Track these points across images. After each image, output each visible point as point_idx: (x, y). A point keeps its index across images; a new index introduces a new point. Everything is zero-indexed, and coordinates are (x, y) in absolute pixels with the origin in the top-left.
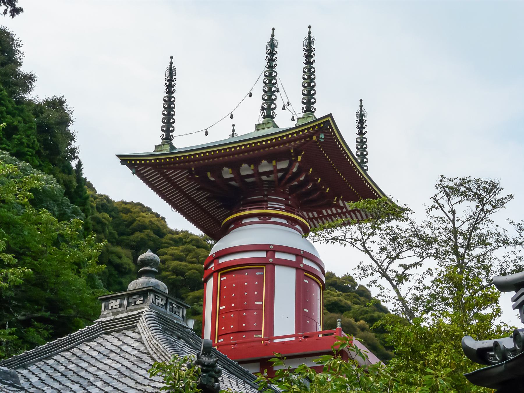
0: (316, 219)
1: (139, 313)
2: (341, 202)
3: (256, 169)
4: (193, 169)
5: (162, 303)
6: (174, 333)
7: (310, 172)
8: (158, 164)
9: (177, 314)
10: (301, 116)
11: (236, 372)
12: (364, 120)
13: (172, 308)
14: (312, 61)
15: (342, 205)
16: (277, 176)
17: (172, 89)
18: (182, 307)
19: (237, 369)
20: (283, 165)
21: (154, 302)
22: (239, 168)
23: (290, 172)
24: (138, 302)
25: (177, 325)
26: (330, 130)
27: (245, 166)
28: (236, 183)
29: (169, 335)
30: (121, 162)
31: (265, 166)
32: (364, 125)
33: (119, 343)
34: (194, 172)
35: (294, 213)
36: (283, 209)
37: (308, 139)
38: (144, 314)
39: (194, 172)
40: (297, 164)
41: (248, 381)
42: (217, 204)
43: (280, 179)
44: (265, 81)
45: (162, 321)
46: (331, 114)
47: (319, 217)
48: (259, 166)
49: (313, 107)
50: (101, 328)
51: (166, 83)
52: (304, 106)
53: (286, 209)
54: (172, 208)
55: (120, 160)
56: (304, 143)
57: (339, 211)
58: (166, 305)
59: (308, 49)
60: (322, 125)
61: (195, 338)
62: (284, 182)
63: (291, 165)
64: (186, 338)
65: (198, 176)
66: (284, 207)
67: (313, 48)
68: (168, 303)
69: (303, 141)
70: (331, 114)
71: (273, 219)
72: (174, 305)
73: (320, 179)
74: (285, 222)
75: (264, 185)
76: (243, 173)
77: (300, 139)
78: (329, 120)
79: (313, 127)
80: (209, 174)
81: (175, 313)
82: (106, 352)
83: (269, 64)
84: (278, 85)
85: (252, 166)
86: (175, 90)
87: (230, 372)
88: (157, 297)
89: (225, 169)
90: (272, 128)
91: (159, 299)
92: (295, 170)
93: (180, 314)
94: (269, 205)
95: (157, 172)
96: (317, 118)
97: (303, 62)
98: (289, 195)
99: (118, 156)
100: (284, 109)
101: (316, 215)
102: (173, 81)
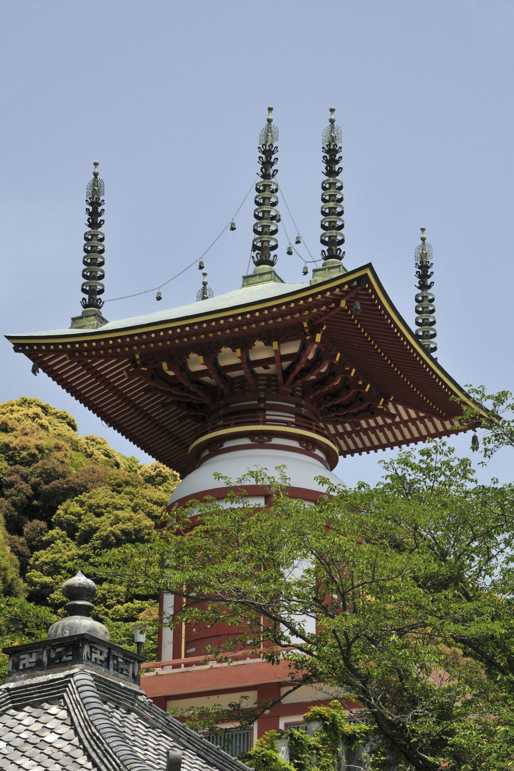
1: (67, 677)
3: (245, 356)
4: (137, 357)
5: (102, 658)
6: (120, 704)
7: (337, 359)
8: (78, 350)
9: (125, 672)
11: (218, 762)
13: (118, 664)
14: (336, 170)
15: (393, 411)
16: (281, 367)
17: (99, 219)
18: (132, 661)
19: (219, 756)
21: (90, 657)
23: (303, 360)
25: (125, 691)
26: (370, 291)
30: (14, 348)
31: (259, 350)
32: (430, 271)
34: (138, 362)
35: (310, 430)
36: (292, 423)
37: (333, 305)
38: (76, 678)
39: (138, 362)
40: (315, 346)
42: (180, 413)
43: (286, 373)
44: (257, 200)
45: (102, 687)
46: (371, 263)
48: (250, 351)
49: (339, 249)
50: (7, 700)
53: (297, 423)
55: (14, 344)
56: (325, 312)
57: (389, 421)
58: (107, 660)
60: (355, 283)
61: (153, 710)
62: (292, 376)
64: (140, 711)
65: (146, 369)
66: (294, 420)
68: (111, 657)
69: (324, 308)
70: (371, 263)
71: (276, 441)
73: (354, 370)
74: (295, 444)
75: (260, 382)
76: (224, 362)
77: (318, 305)
78: (366, 275)
80: (165, 366)
82: (18, 742)
83: (263, 170)
84: (280, 209)
85: (238, 351)
86: (103, 221)
88: (93, 650)
89: (193, 356)
90: (271, 284)
91: (96, 651)
92: (311, 356)
93: (129, 673)
94: (267, 417)
96: (349, 270)
97: (322, 172)
98: (303, 398)
99: (9, 338)
100: (290, 253)
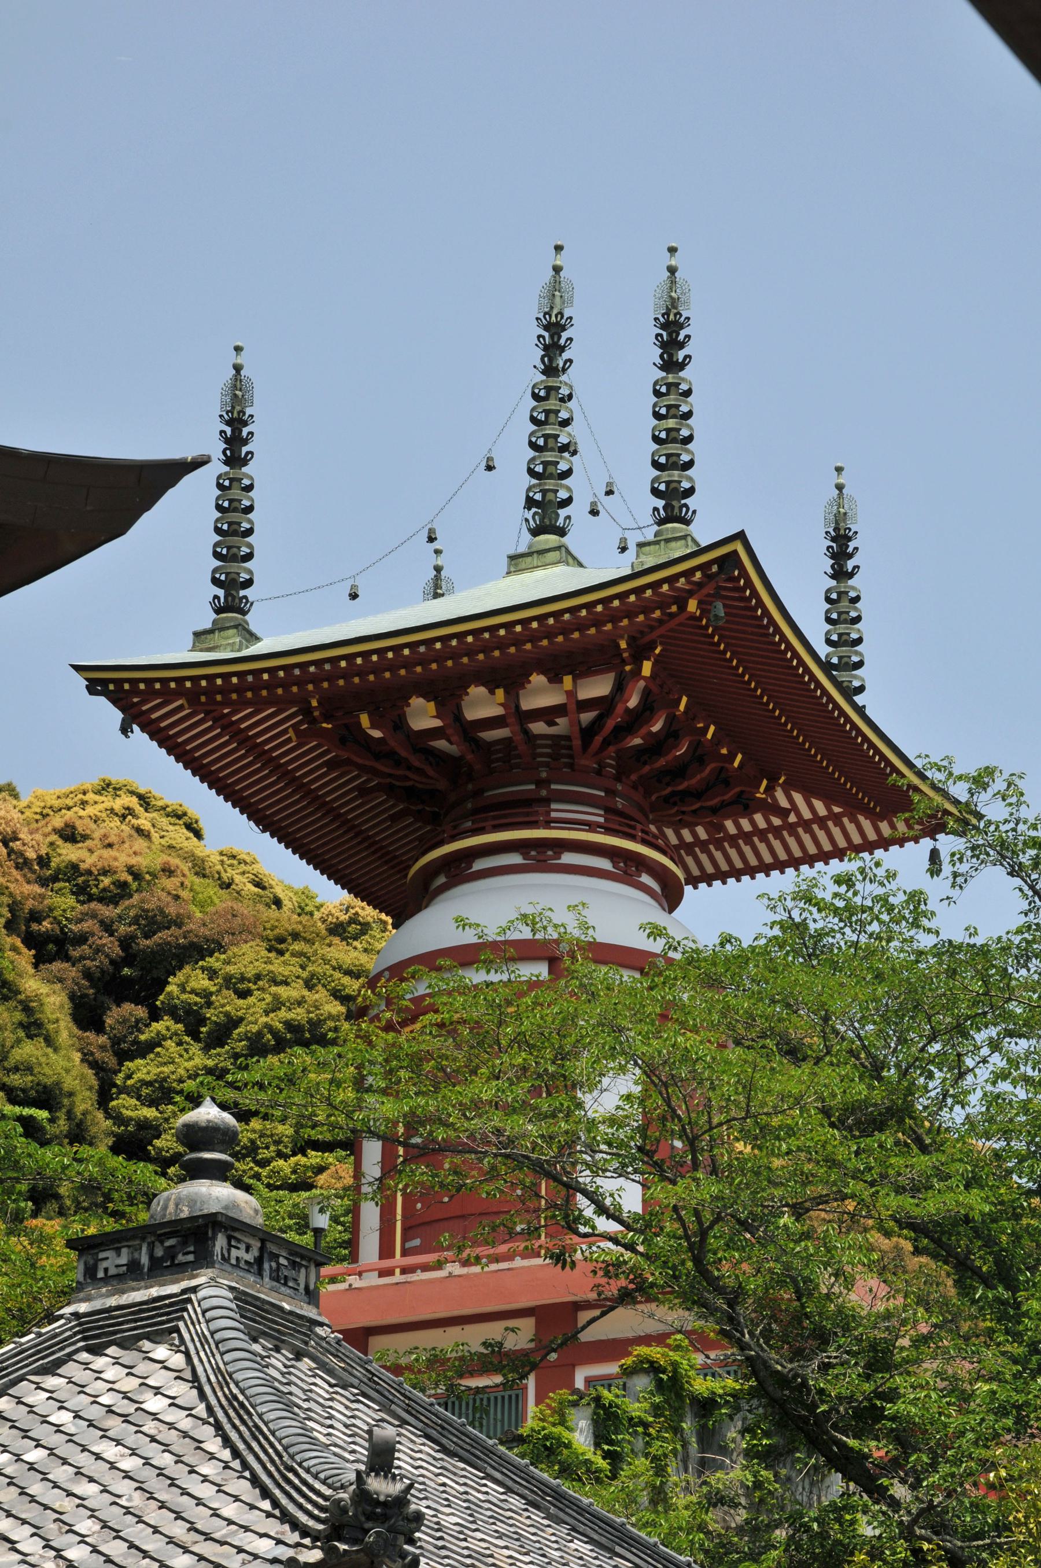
0: (703, 845)
1: (184, 1291)
2: (780, 796)
3: (512, 703)
6: (283, 1341)
7: (682, 707)
8: (205, 692)
9: (291, 1284)
10: (649, 535)
12: (850, 529)
13: (278, 1269)
14: (680, 360)
15: (784, 803)
18: (304, 1263)
20: (598, 687)
21: (226, 1255)
22: (460, 698)
23: (619, 709)
24: (181, 1258)
25: (291, 1318)
27: (477, 691)
28: (451, 743)
29: (271, 1349)
30: (87, 687)
31: (539, 691)
32: (852, 545)
33: (130, 1384)
34: (316, 714)
35: (632, 837)
37: (674, 608)
38: (201, 1294)
39: (316, 714)
40: (642, 684)
41: (498, 1475)
43: (588, 733)
45: (250, 1311)
46: (743, 531)
47: (711, 840)
49: (686, 505)
50: (75, 1334)
51: (225, 432)
52: (660, 503)
53: (607, 825)
54: (251, 823)
55: (87, 679)
56: (660, 622)
57: (777, 821)
58: (259, 1261)
59: (667, 321)
60: (715, 568)
62: (598, 739)
63: (620, 688)
65: (330, 726)
66: (601, 820)
67: (682, 319)
68: (266, 1255)
69: (657, 614)
70: (743, 531)
71: (569, 858)
72: (282, 1261)
73: (712, 728)
74: (604, 864)
75: (539, 750)
77: (646, 609)
78: (735, 552)
79: (688, 574)
80: (365, 720)
81: (285, 1284)
82: (95, 1413)
83: (546, 359)
84: (576, 432)
85: (500, 693)
87: (444, 1450)
89: (417, 702)
92: (633, 703)
93: (298, 1285)
94: (553, 815)
95: (202, 715)
98: (618, 778)
99: (78, 668)
101: (702, 833)
102: (245, 424)
